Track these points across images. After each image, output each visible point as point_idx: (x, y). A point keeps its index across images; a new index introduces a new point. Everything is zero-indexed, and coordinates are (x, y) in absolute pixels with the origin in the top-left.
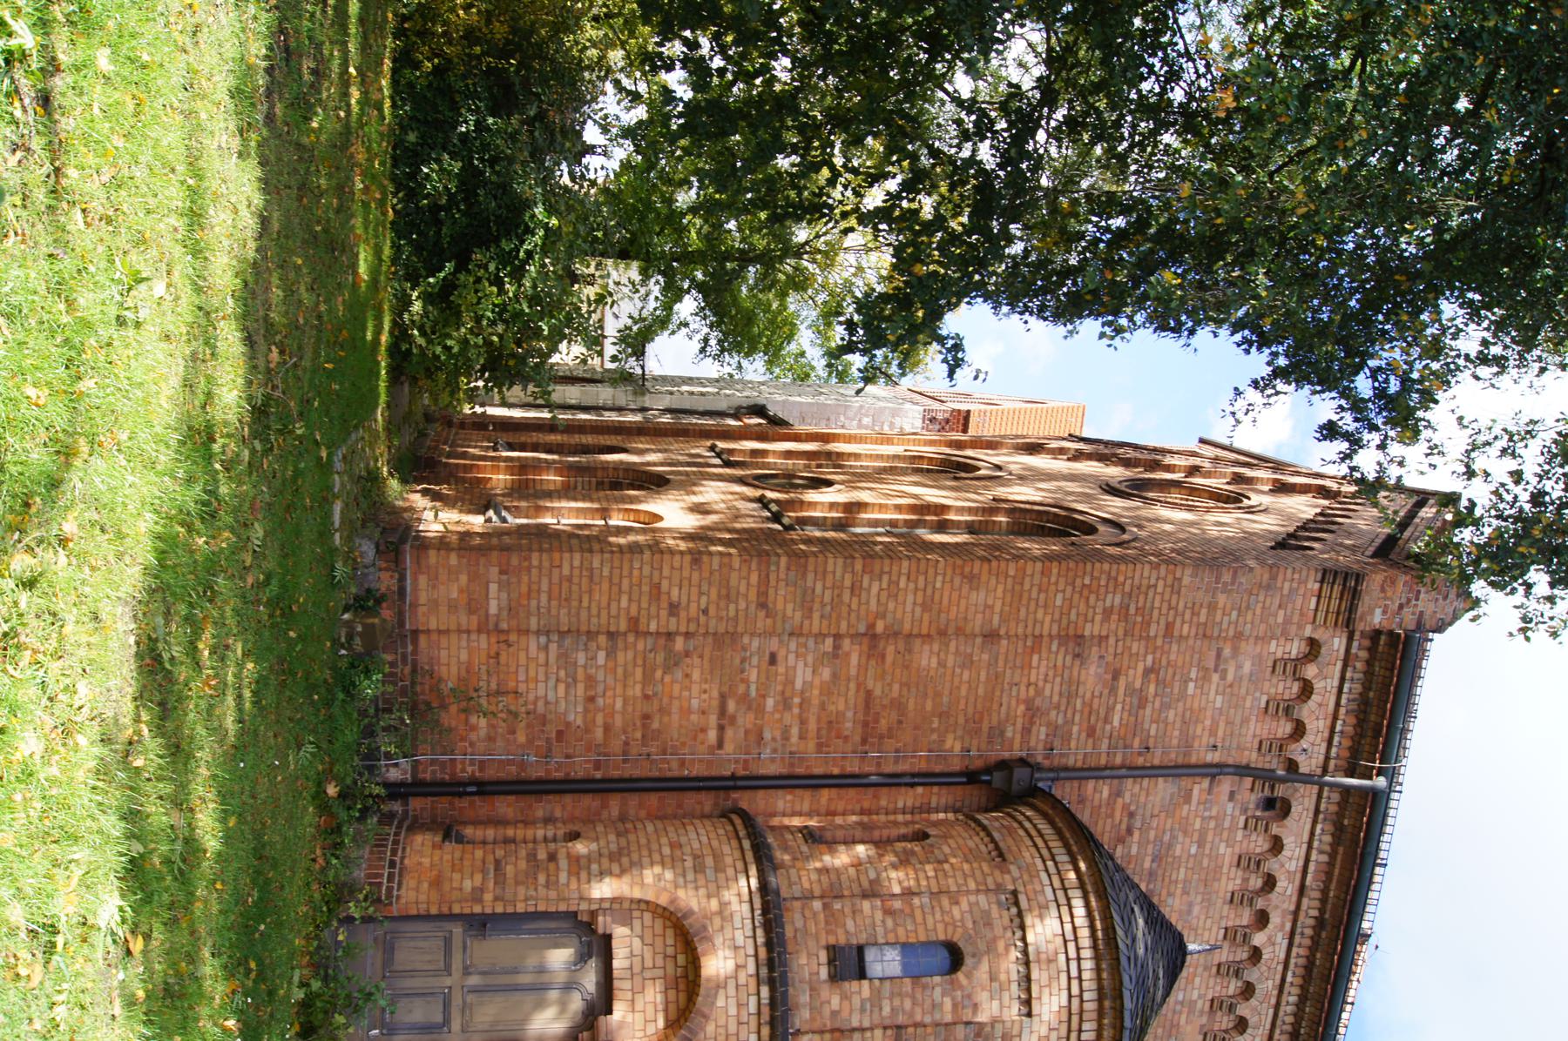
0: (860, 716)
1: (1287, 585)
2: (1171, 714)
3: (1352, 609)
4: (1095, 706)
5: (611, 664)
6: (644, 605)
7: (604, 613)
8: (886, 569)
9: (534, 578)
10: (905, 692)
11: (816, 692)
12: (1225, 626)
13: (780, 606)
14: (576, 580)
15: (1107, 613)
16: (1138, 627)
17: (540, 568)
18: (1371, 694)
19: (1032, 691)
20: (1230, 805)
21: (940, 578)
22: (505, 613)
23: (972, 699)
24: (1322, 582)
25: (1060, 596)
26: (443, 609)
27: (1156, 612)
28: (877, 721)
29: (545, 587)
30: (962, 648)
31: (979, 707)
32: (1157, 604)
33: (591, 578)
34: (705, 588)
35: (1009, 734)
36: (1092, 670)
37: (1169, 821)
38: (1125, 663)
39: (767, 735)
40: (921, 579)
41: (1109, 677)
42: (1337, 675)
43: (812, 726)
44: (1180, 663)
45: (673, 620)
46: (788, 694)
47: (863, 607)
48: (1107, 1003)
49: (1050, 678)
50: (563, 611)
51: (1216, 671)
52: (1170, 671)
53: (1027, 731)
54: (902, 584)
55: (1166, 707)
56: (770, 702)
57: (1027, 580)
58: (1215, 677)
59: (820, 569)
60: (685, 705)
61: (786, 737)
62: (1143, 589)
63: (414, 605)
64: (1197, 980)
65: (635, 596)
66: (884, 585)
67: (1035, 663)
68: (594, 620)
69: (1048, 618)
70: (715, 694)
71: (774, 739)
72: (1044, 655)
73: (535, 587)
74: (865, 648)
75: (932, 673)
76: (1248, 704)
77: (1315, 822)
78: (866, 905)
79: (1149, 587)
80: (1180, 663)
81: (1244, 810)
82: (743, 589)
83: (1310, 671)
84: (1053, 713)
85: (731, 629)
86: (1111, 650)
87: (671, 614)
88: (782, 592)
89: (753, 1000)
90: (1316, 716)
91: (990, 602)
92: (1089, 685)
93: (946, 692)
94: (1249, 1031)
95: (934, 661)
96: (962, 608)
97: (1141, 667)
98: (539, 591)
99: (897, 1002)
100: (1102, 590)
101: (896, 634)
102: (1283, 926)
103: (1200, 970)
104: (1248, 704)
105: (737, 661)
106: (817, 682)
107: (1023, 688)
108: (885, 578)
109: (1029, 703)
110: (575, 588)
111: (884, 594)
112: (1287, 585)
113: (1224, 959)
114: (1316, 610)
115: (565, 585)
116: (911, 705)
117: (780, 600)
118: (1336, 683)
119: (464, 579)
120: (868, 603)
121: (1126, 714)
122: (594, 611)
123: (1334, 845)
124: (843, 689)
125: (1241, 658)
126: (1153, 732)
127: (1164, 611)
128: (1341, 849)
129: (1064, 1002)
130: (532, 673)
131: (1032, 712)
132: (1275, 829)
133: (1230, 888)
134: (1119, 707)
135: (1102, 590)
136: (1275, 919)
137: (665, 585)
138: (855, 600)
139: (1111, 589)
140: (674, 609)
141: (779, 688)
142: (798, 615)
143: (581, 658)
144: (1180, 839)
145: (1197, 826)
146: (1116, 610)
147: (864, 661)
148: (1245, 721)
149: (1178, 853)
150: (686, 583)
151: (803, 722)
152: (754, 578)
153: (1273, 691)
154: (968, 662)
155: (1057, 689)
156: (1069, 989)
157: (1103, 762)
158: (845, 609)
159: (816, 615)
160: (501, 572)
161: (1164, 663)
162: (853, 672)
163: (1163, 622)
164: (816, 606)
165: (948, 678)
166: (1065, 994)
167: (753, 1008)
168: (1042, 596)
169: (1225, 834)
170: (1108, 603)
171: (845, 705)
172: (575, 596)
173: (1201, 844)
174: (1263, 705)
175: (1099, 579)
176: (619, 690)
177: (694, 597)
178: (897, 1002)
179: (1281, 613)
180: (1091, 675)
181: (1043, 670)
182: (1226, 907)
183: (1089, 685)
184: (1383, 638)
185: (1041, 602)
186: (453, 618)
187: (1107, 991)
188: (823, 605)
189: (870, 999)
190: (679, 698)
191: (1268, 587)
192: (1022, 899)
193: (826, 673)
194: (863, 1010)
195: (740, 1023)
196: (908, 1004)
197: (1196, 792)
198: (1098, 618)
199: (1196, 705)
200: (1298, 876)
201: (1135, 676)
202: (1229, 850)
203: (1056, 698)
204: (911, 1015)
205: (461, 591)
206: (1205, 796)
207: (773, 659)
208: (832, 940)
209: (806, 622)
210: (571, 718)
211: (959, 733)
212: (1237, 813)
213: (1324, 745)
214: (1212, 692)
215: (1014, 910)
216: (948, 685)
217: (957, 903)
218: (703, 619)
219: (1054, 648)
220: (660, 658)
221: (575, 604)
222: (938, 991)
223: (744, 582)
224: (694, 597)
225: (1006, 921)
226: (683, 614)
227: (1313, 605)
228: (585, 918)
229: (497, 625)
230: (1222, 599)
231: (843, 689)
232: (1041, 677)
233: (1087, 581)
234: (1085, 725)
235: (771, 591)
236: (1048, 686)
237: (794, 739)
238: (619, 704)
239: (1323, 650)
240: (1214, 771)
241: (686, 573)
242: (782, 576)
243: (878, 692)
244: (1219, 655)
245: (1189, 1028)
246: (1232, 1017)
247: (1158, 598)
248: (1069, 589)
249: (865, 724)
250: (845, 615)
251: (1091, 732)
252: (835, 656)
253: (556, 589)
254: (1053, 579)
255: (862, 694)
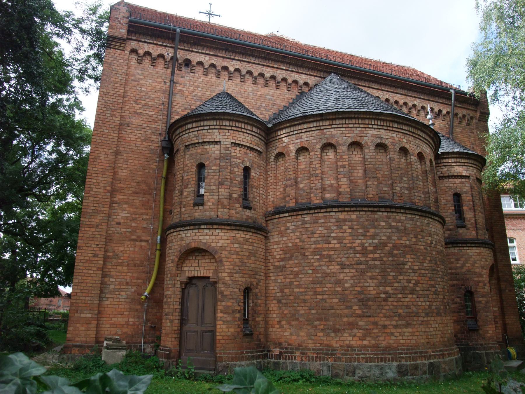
0: (141, 195)
1: (110, 59)
2: (152, 96)
3: (119, 39)
4: (146, 120)
5: (115, 277)
6: (93, 265)
7: (95, 279)
8: (89, 186)
9: (80, 301)
10: (135, 181)
11: (131, 210)
12: (122, 78)
13: (98, 221)
14: (82, 288)
15: (112, 115)
16: (119, 106)
17: (76, 299)
18: (150, 33)
19: (139, 140)
20: (186, 77)
21: (94, 169)
22: (92, 312)
23: (140, 159)
24: (111, 48)
25: (105, 131)
26: (89, 332)
27: (114, 100)
28: (144, 190)
29: (83, 298)
30: (121, 162)
31: (142, 157)
32: (112, 100)
33: (81, 283)
34: (89, 245)
35: (153, 147)
36: (133, 121)
37: (189, 97)
38: (133, 110)
39: (145, 226)
40: (93, 175)
41: (137, 115)
42: (143, 44)
43: (143, 211)
44: (135, 93)
45: (99, 256)
46: (131, 219)
47: (101, 194)
48: (217, 117)
49: (135, 134)
50: (93, 292)
51: (139, 82)
52: (137, 96)
53: (152, 142)
54: (95, 181)
55: (149, 98)
56: (133, 224)
57: (98, 141)
58: (141, 82)
59: (87, 207)
60: (132, 252)
61: (147, 220)
62: (106, 104)
63: (86, 342)
64: (246, 88)
65: (90, 268)
66: (94, 187)
67: (129, 139)
68: (97, 282)
69: (112, 134)
70: (129, 243)
71: (147, 224)
72: (127, 136)
73: (83, 301)
74: (118, 193)
75: (129, 172)
76: (152, 72)
77: (192, 51)
78: (185, 194)
79: (105, 102)
80: (135, 93)
81: (188, 73)
82: (91, 233)
83: (141, 52)
84: (147, 133)
85: (105, 237)
86: (128, 114)
87: (97, 257)
88: (93, 220)
89: (206, 231)
90: (156, 51)
91: (104, 153)
92: (139, 121)
93: (136, 167)
94: (263, 72)
95: (124, 171)
96: (106, 162)
97: (134, 105)
98: (85, 300)
99: (212, 184)
100: (104, 117)
101: (112, 183)
102: (228, 62)
103: (242, 88)
104: (152, 72)
105: (118, 235)
106: (128, 209)
107: (138, 143)
108: (92, 186)
109: (142, 141)
110: (85, 288)
111: (97, 187)
112: (110, 59)
113: (239, 80)
114: (120, 50)
115: (83, 291)
116: (139, 179)
117: (96, 221)
118: (146, 44)
119: (78, 325)
120: (100, 192)
121: (150, 110)
122: (94, 282)
123: (201, 46)
124: (131, 201)
125: (135, 74)
126: (158, 102)
127: (114, 97)
128: (202, 43)
129: (217, 131)
130: (116, 303)
131: (146, 140)
132: (194, 63)
133: (215, 78)
134: (147, 112)
135: (104, 117)
136: (225, 64)
137: (86, 258)
138: (99, 196)
139: (104, 114)
140: (95, 256)
141: (129, 221)
142: (102, 215)
143: (112, 286)
144: (196, 93)
145: (192, 88)
146: (112, 113)
147: (122, 194)
148: (157, 73)
149: (200, 94)
150: (87, 252)
151: (142, 214)
152: (87, 229)
153: (148, 64)
154: (127, 160)
155: (139, 132)
156: (213, 129)
157: (166, 118)
158: (101, 200)
159: (102, 209)
160: (77, 313)
161: (134, 98)
162: (125, 197)
163: (118, 98)
164: (99, 209)
165: (131, 167)
166: (214, 131)
167: (208, 231)
168: (104, 136)
169: (195, 79)
170: (109, 115)
171: (137, 201)
172: (88, 288)
173: (199, 87)
174: (152, 67)
175: (100, 118)
176: (125, 274)
177: (92, 249)
178: (212, 184)
179: (120, 61)
180: (135, 121)
181: (132, 136)
182: (221, 79)
183: (139, 121)
184: (131, 29)
185: (107, 136)
186: (92, 329)
187: (213, 117)
188: (99, 207)
189: (210, 193)
190: (129, 254)
191: (110, 65)
192: (188, 143)
193: (125, 206)
194: (213, 195)
195: (212, 235)
196: (213, 181)
197: (179, 88)
198: (114, 118)
199: (150, 88)
200: (211, 57)
201: (137, 107)
202: (201, 78)
203: (142, 132)
204: (216, 179)
205: (82, 326)
206: (182, 86)
207: (119, 223)
208: (192, 205)
209: (105, 212)
210: (133, 290)
211: (151, 163)
212: (189, 75)
213: (167, 48)
214: (146, 83)
215: (190, 146)
216: (134, 167)
217: (187, 165)
218: (100, 246)
219: (124, 132)
220: (115, 261)
221: (90, 288)
222: (210, 171)
223: (88, 232)
224: (92, 249)
225: (193, 149)
226: (97, 252)
227: (119, 51)
228: (183, 286)
229: (95, 314)
230: (112, 79)
231: (131, 201)
232: (134, 137)
233: (101, 122)
234: (153, 123)
235: (93, 223)
236: (138, 135)
237: (147, 217)
238: (130, 274)
239: (134, 48)
240: (173, 82)
241: (83, 251)
242: (87, 220)
243: (133, 189)
244: (134, 81)
245: (262, 91)
246: (259, 77)
247: (109, 99)
248: (103, 127)
249: (144, 194)
250: (103, 200)
251: (155, 121)
252: (119, 203)
253: (84, 295)
254: (99, 133)
255: (133, 195)
